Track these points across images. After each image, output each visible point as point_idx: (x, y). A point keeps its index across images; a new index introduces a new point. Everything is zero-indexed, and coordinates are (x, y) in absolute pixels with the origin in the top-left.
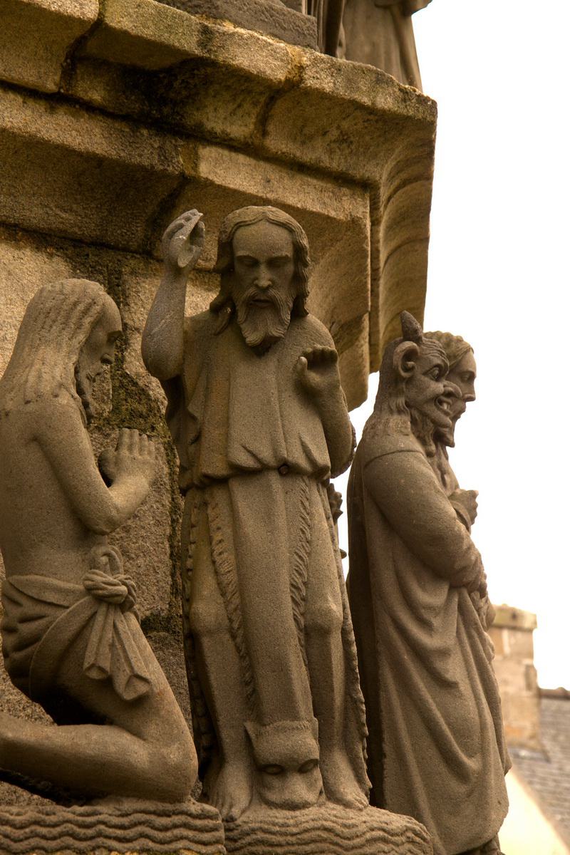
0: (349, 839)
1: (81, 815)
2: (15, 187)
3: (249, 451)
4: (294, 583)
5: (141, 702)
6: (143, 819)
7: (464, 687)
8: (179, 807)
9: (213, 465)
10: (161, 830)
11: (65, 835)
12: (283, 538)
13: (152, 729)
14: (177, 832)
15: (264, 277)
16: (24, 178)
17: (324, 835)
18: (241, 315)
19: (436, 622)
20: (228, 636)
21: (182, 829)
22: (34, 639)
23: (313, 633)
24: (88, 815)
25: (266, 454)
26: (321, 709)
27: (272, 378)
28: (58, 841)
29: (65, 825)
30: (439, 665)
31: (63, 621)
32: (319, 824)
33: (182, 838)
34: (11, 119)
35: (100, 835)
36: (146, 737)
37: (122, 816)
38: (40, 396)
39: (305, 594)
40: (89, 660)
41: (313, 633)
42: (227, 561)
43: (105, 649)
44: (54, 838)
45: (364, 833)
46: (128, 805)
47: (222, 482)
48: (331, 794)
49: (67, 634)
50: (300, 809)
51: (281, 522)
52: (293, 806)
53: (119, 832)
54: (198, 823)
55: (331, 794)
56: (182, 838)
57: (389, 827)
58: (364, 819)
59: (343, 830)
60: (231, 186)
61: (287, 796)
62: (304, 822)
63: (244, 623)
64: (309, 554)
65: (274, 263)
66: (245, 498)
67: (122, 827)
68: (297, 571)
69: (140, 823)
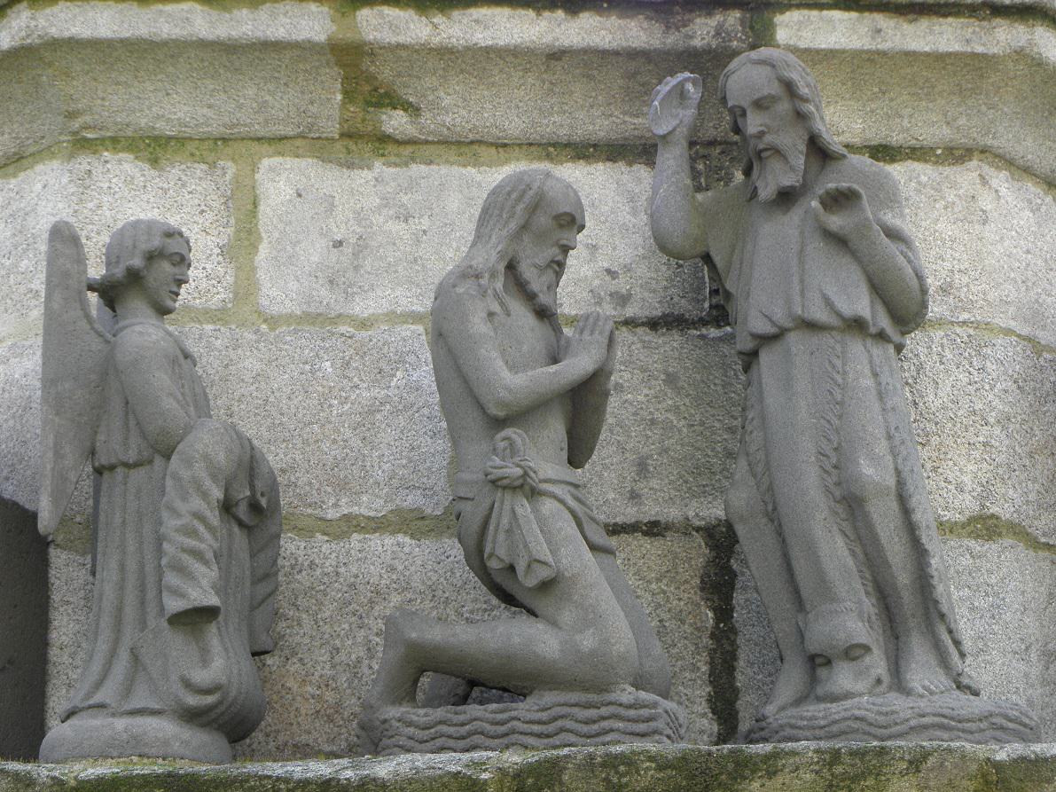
0: (885, 727)
1: (494, 712)
2: (567, 104)
3: (766, 316)
4: (822, 451)
6: (563, 713)
8: (612, 697)
10: (586, 723)
11: (474, 734)
13: (567, 616)
14: (605, 724)
16: (572, 92)
17: (856, 725)
20: (764, 520)
21: (611, 721)
24: (502, 712)
28: (468, 740)
29: (474, 723)
32: (849, 714)
33: (612, 730)
34: (521, 35)
35: (513, 732)
36: (560, 626)
37: (543, 710)
43: (501, 537)
44: (463, 738)
45: (907, 720)
50: (841, 700)
52: (834, 698)
53: (536, 728)
54: (632, 713)
56: (612, 730)
57: (954, 712)
58: (911, 705)
59: (877, 717)
60: (823, 46)
62: (835, 713)
64: (840, 417)
65: (759, 104)
67: (539, 722)
68: (825, 437)
69: (562, 717)
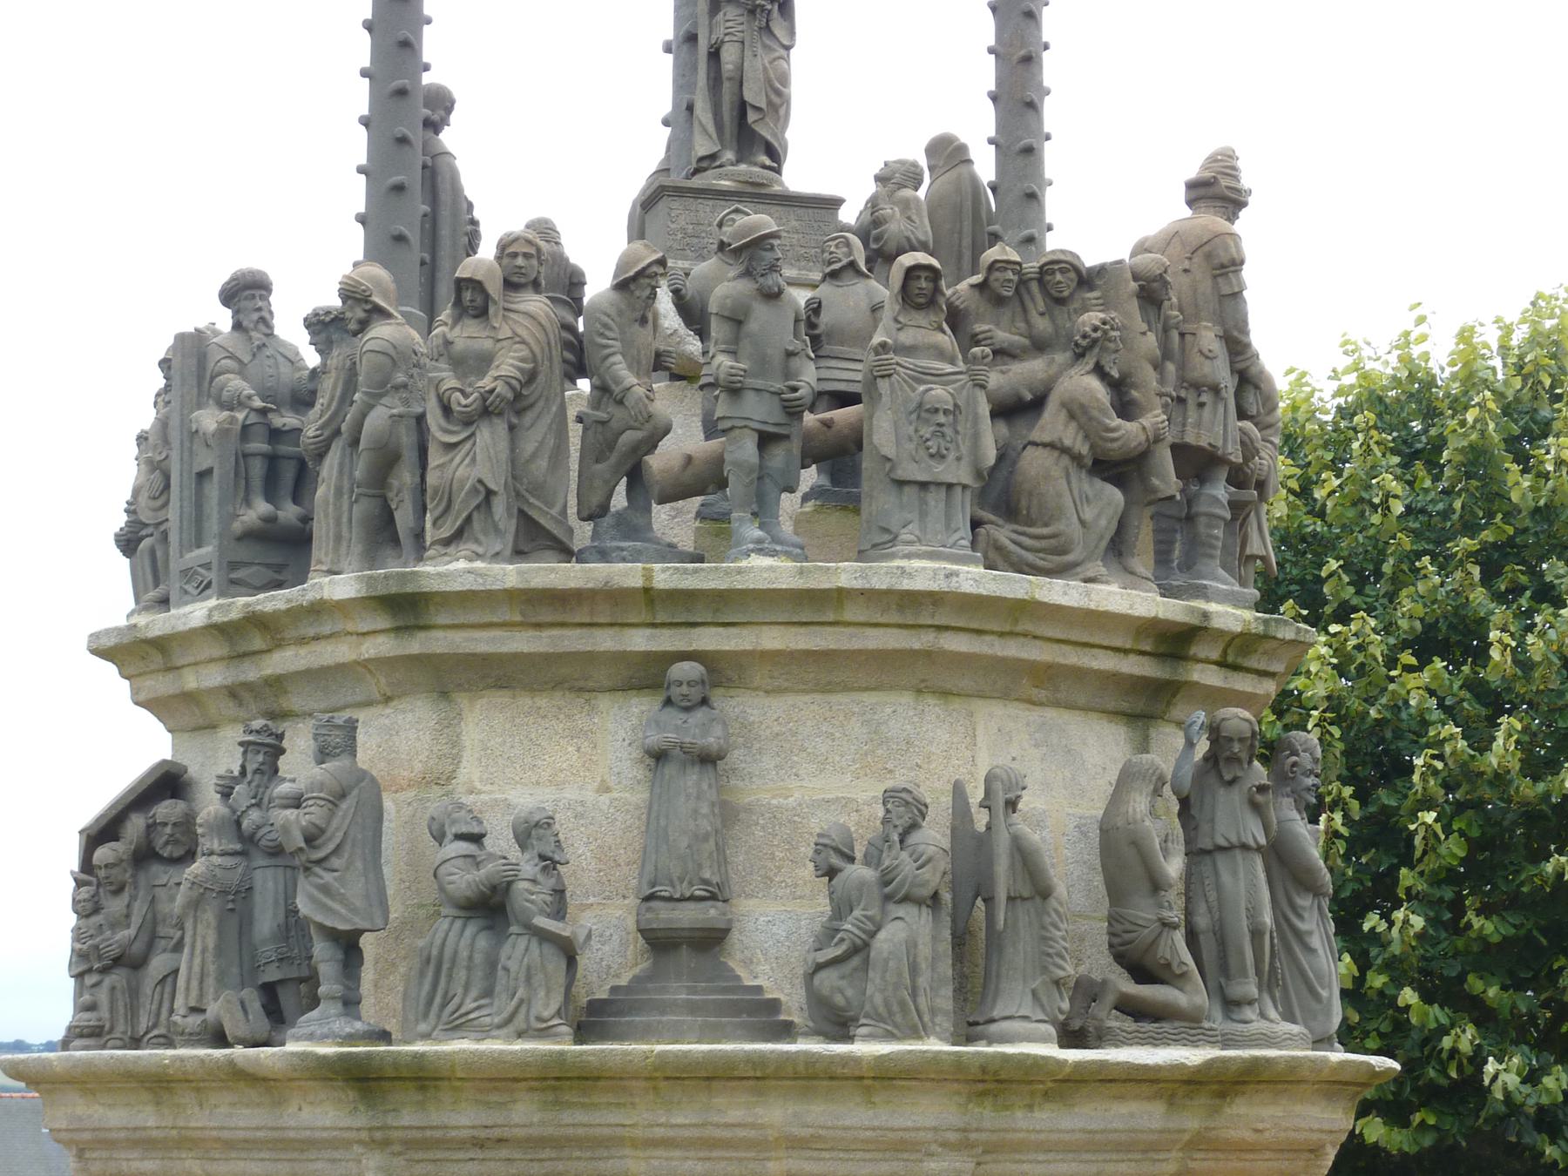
5: (1183, 975)
7: (1321, 952)
9: (1205, 843)
12: (1242, 884)
13: (1188, 988)
15: (1236, 747)
18: (1221, 764)
19: (1306, 915)
22: (1130, 942)
23: (1256, 934)
25: (1234, 840)
26: (1259, 972)
27: (1237, 798)
30: (1307, 939)
31: (1146, 934)
38: (1135, 822)
39: (1253, 913)
40: (1160, 954)
41: (1256, 934)
42: (1212, 896)
46: (1177, 1024)
47: (1209, 852)
48: (1263, 1015)
49: (1149, 940)
51: (1242, 875)
52: (1246, 1022)
55: (1263, 1015)
61: (1242, 1017)
63: (1222, 927)
65: (1241, 740)
66: (1222, 861)
